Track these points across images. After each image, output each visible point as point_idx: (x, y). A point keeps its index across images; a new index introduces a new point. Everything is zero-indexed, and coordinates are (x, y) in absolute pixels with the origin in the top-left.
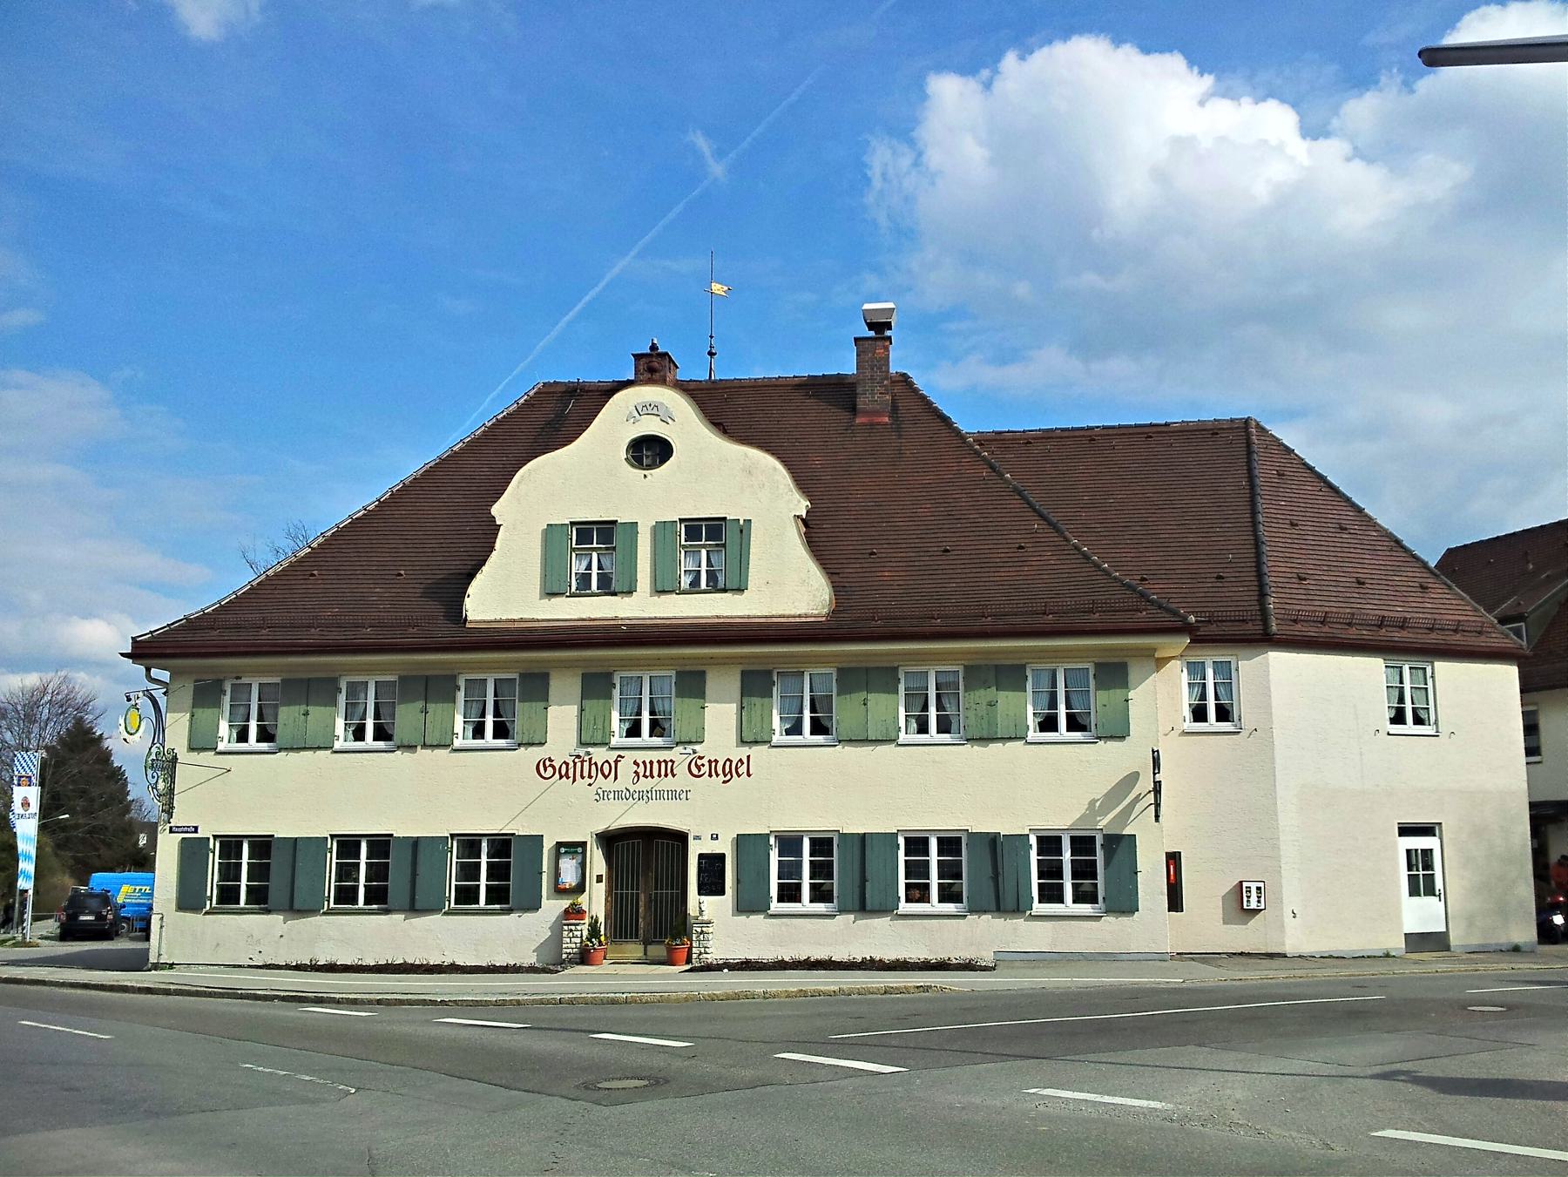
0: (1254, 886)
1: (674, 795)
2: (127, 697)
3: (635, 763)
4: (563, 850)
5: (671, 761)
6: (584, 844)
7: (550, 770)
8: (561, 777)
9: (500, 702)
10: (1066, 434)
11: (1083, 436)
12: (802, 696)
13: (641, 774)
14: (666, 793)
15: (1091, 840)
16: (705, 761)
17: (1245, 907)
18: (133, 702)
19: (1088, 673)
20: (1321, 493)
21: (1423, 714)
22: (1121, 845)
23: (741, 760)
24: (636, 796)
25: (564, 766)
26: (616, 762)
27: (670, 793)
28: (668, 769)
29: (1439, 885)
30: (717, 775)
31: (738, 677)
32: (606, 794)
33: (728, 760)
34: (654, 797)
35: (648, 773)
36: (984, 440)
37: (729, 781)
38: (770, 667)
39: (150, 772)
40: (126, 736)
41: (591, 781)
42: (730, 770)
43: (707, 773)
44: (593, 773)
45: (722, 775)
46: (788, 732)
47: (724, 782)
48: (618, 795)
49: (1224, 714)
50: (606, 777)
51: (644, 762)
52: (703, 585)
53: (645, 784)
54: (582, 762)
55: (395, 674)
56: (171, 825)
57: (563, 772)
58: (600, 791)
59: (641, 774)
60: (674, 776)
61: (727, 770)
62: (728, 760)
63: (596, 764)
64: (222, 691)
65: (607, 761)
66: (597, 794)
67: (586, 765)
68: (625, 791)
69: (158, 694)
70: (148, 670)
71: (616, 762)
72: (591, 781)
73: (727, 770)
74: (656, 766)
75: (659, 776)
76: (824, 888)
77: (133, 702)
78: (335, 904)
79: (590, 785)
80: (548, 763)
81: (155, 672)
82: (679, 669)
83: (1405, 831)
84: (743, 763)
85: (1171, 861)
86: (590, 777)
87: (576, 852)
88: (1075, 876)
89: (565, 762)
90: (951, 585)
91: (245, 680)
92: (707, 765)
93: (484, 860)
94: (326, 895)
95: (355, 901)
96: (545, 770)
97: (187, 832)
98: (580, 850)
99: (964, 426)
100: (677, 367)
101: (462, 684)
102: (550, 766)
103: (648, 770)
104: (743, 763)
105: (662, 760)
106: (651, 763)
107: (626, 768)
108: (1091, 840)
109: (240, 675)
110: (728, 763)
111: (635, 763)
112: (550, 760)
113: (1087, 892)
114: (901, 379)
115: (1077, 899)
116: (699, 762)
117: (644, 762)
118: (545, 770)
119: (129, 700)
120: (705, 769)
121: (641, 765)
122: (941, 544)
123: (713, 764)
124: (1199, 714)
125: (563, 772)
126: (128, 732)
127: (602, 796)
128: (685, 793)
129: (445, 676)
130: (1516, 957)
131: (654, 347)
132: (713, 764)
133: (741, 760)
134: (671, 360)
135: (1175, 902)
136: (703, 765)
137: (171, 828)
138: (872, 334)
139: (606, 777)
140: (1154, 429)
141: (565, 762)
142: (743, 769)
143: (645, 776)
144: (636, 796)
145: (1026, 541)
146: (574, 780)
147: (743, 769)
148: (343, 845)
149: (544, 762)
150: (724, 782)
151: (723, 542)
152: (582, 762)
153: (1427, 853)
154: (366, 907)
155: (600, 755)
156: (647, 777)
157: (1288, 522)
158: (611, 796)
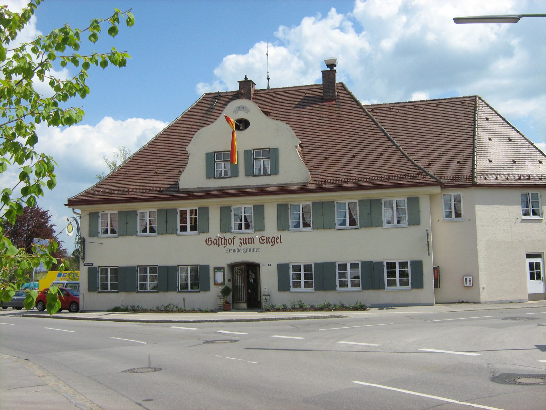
0: (468, 278)
1: (255, 250)
2: (68, 220)
3: (240, 239)
4: (216, 270)
5: (253, 238)
6: (223, 268)
7: (210, 242)
8: (214, 245)
9: (112, 221)
10: (406, 104)
11: (412, 105)
12: (300, 213)
13: (242, 243)
14: (251, 250)
15: (299, 266)
16: (265, 238)
17: (465, 285)
18: (70, 222)
19: (405, 202)
20: (503, 125)
21: (537, 212)
22: (417, 265)
23: (278, 237)
24: (241, 251)
25: (215, 241)
26: (233, 239)
27: (253, 250)
28: (251, 241)
29: (542, 276)
30: (270, 243)
31: (276, 206)
32: (230, 250)
33: (273, 237)
34: (247, 251)
35: (245, 243)
36: (373, 108)
37: (274, 245)
38: (288, 203)
39: (76, 245)
40: (68, 233)
41: (225, 246)
42: (274, 241)
43: (280, 242)
44: (226, 243)
45: (271, 243)
46: (341, 225)
47: (272, 245)
48: (234, 251)
49: (458, 215)
50: (230, 244)
51: (243, 239)
52: (262, 173)
53: (244, 246)
54: (221, 239)
55: (357, 200)
56: (84, 263)
57: (215, 243)
58: (228, 249)
59: (242, 243)
60: (254, 243)
61: (273, 241)
62: (273, 237)
63: (226, 239)
64: (137, 215)
65: (230, 239)
66: (227, 250)
67: (223, 240)
68: (237, 249)
69: (78, 219)
70: (73, 209)
71: (233, 239)
72: (225, 246)
73: (273, 241)
74: (247, 240)
75: (249, 243)
76: (309, 283)
77: (70, 222)
78: (180, 289)
79: (224, 247)
80: (209, 240)
81: (76, 211)
82: (408, 197)
83: (529, 256)
84: (278, 238)
85: (436, 270)
86: (224, 244)
87: (221, 271)
88: (305, 278)
89: (215, 239)
90: (355, 169)
91: (106, 212)
92: (266, 239)
93: (109, 275)
94: (177, 286)
95: (188, 288)
96: (209, 242)
97: (90, 266)
98: (222, 270)
99: (363, 103)
100: (255, 85)
101: (233, 209)
102: (210, 240)
103: (244, 241)
104: (278, 238)
105: (252, 238)
106: (246, 239)
107: (237, 241)
108: (299, 266)
109: (104, 210)
110: (273, 238)
111: (240, 239)
112: (210, 238)
113: (405, 282)
114: (341, 85)
115: (305, 287)
116: (263, 238)
117: (243, 239)
118: (209, 242)
119: (68, 221)
120: (265, 241)
121: (242, 240)
122: (353, 153)
123: (268, 239)
124: (449, 215)
125: (215, 243)
126: (69, 232)
127: (229, 251)
128: (258, 249)
129: (377, 200)
130: (512, 304)
131: (246, 78)
132: (268, 239)
133: (278, 237)
134: (253, 83)
135: (437, 284)
136: (264, 239)
137: (84, 264)
138: (329, 69)
139: (230, 244)
140: (440, 101)
141: (215, 239)
142: (279, 240)
143: (244, 243)
144: (241, 251)
145: (384, 151)
146: (219, 245)
147: (279, 240)
148: (152, 269)
149: (208, 239)
150: (272, 245)
151: (269, 157)
152: (221, 239)
153: (538, 265)
154: (111, 291)
155: (228, 236)
156: (244, 244)
157: (488, 138)
158: (232, 251)
